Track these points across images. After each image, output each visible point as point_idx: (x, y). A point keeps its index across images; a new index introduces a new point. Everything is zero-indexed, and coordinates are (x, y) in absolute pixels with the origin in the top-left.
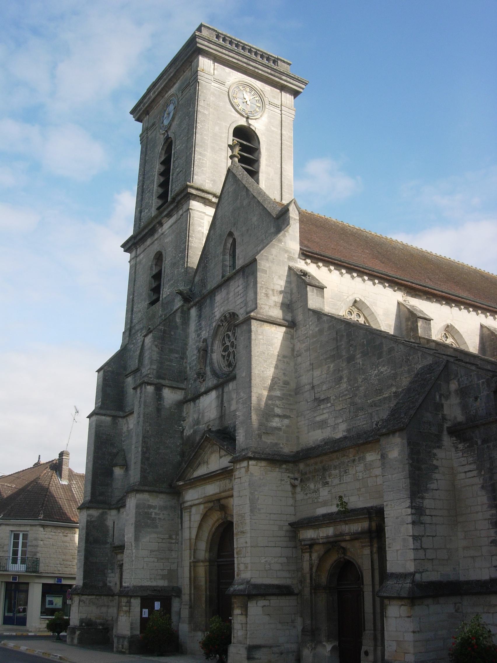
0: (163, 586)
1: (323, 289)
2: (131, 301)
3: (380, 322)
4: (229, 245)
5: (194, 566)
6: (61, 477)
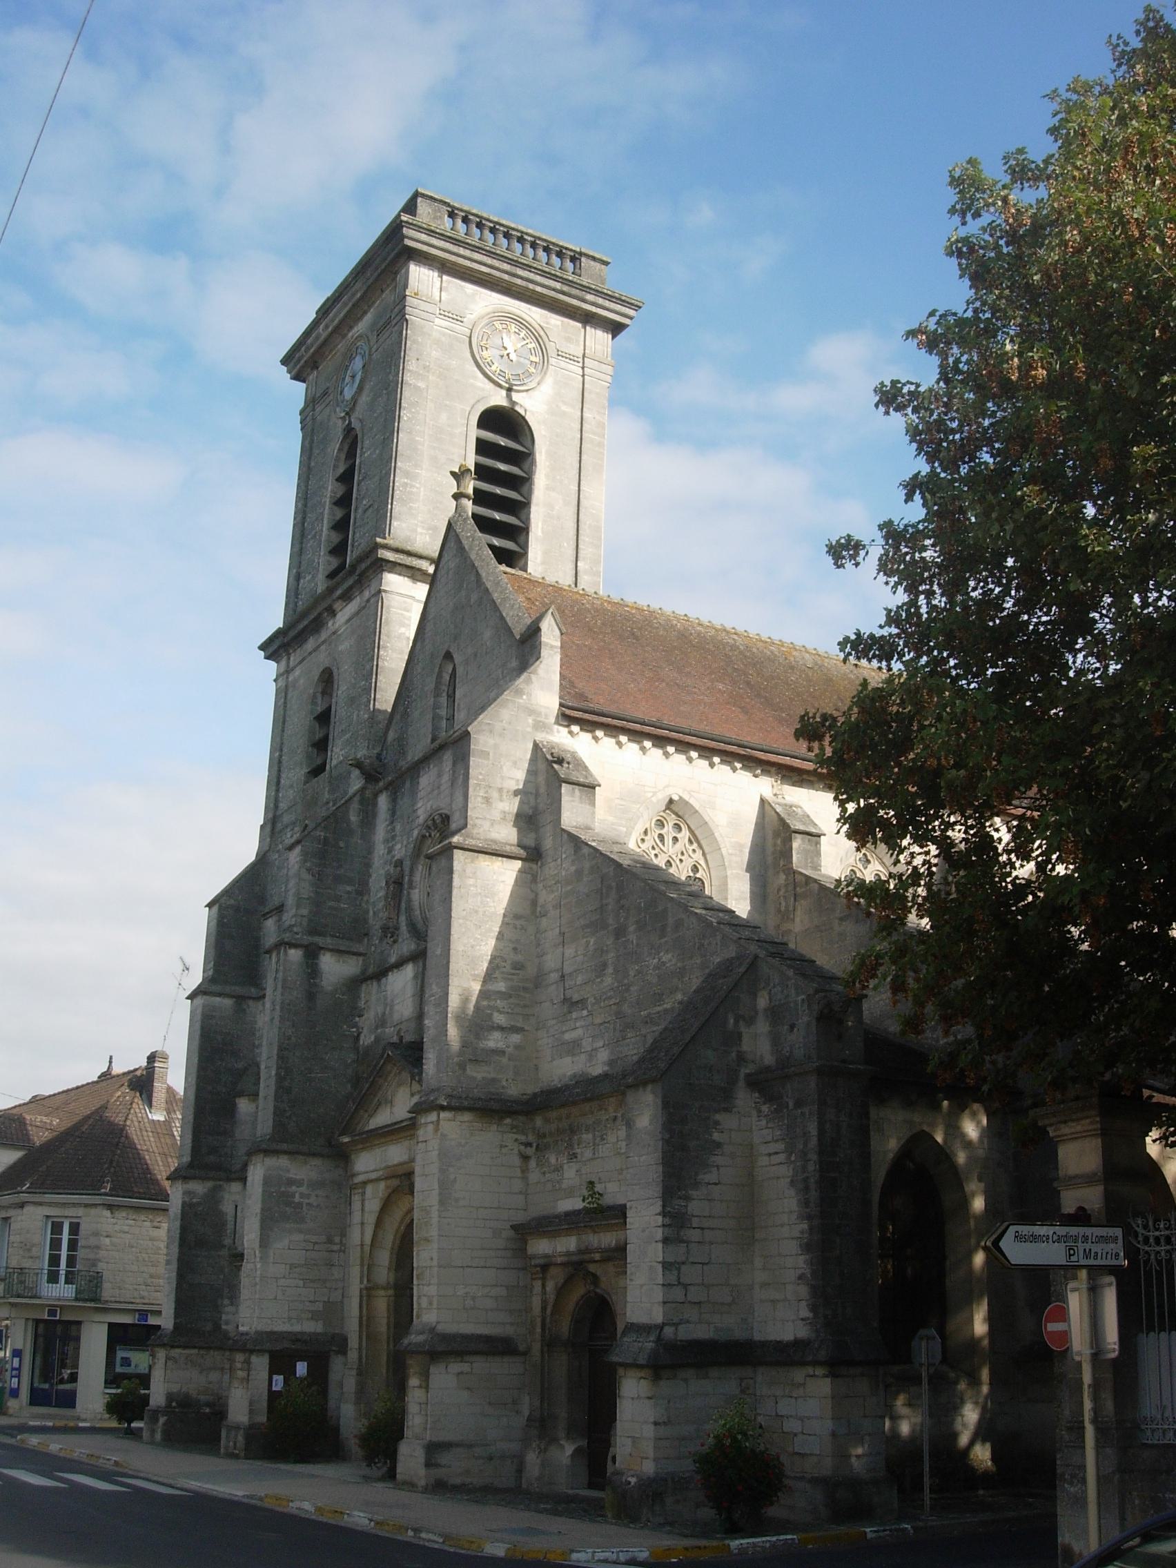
0: (315, 1334)
1: (594, 788)
2: (276, 761)
3: (719, 839)
4: (447, 677)
5: (369, 1296)
6: (150, 1106)
